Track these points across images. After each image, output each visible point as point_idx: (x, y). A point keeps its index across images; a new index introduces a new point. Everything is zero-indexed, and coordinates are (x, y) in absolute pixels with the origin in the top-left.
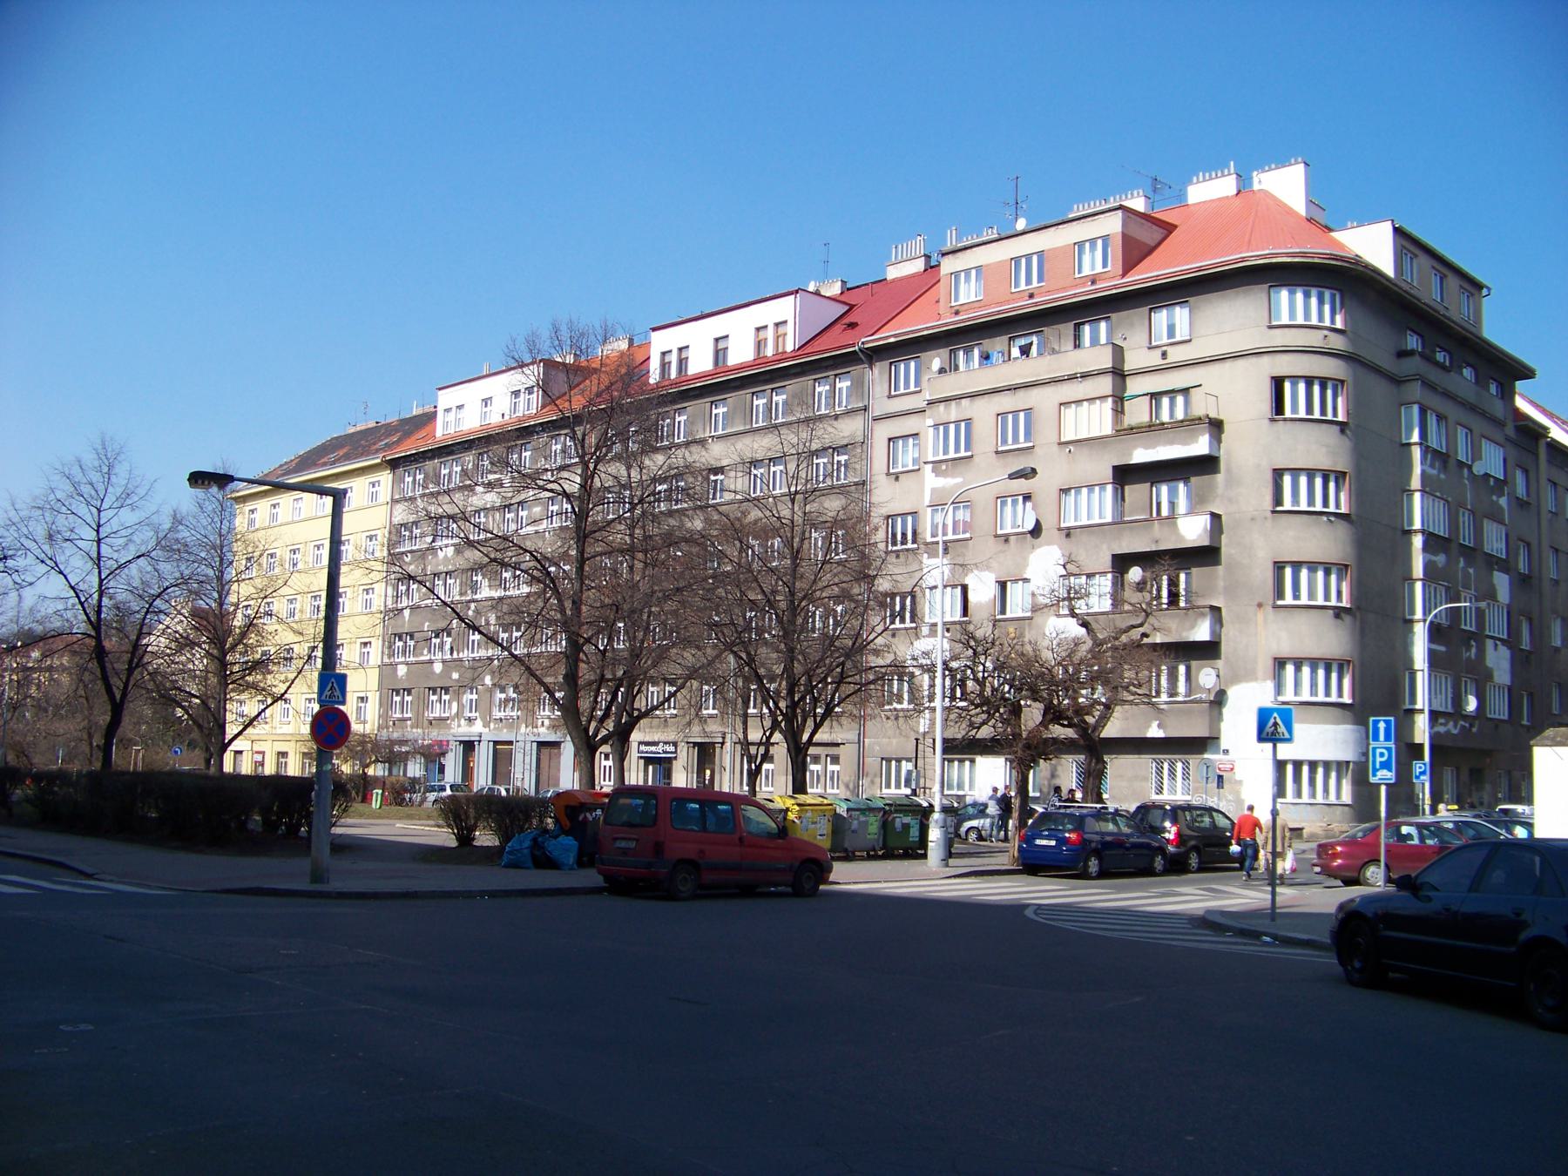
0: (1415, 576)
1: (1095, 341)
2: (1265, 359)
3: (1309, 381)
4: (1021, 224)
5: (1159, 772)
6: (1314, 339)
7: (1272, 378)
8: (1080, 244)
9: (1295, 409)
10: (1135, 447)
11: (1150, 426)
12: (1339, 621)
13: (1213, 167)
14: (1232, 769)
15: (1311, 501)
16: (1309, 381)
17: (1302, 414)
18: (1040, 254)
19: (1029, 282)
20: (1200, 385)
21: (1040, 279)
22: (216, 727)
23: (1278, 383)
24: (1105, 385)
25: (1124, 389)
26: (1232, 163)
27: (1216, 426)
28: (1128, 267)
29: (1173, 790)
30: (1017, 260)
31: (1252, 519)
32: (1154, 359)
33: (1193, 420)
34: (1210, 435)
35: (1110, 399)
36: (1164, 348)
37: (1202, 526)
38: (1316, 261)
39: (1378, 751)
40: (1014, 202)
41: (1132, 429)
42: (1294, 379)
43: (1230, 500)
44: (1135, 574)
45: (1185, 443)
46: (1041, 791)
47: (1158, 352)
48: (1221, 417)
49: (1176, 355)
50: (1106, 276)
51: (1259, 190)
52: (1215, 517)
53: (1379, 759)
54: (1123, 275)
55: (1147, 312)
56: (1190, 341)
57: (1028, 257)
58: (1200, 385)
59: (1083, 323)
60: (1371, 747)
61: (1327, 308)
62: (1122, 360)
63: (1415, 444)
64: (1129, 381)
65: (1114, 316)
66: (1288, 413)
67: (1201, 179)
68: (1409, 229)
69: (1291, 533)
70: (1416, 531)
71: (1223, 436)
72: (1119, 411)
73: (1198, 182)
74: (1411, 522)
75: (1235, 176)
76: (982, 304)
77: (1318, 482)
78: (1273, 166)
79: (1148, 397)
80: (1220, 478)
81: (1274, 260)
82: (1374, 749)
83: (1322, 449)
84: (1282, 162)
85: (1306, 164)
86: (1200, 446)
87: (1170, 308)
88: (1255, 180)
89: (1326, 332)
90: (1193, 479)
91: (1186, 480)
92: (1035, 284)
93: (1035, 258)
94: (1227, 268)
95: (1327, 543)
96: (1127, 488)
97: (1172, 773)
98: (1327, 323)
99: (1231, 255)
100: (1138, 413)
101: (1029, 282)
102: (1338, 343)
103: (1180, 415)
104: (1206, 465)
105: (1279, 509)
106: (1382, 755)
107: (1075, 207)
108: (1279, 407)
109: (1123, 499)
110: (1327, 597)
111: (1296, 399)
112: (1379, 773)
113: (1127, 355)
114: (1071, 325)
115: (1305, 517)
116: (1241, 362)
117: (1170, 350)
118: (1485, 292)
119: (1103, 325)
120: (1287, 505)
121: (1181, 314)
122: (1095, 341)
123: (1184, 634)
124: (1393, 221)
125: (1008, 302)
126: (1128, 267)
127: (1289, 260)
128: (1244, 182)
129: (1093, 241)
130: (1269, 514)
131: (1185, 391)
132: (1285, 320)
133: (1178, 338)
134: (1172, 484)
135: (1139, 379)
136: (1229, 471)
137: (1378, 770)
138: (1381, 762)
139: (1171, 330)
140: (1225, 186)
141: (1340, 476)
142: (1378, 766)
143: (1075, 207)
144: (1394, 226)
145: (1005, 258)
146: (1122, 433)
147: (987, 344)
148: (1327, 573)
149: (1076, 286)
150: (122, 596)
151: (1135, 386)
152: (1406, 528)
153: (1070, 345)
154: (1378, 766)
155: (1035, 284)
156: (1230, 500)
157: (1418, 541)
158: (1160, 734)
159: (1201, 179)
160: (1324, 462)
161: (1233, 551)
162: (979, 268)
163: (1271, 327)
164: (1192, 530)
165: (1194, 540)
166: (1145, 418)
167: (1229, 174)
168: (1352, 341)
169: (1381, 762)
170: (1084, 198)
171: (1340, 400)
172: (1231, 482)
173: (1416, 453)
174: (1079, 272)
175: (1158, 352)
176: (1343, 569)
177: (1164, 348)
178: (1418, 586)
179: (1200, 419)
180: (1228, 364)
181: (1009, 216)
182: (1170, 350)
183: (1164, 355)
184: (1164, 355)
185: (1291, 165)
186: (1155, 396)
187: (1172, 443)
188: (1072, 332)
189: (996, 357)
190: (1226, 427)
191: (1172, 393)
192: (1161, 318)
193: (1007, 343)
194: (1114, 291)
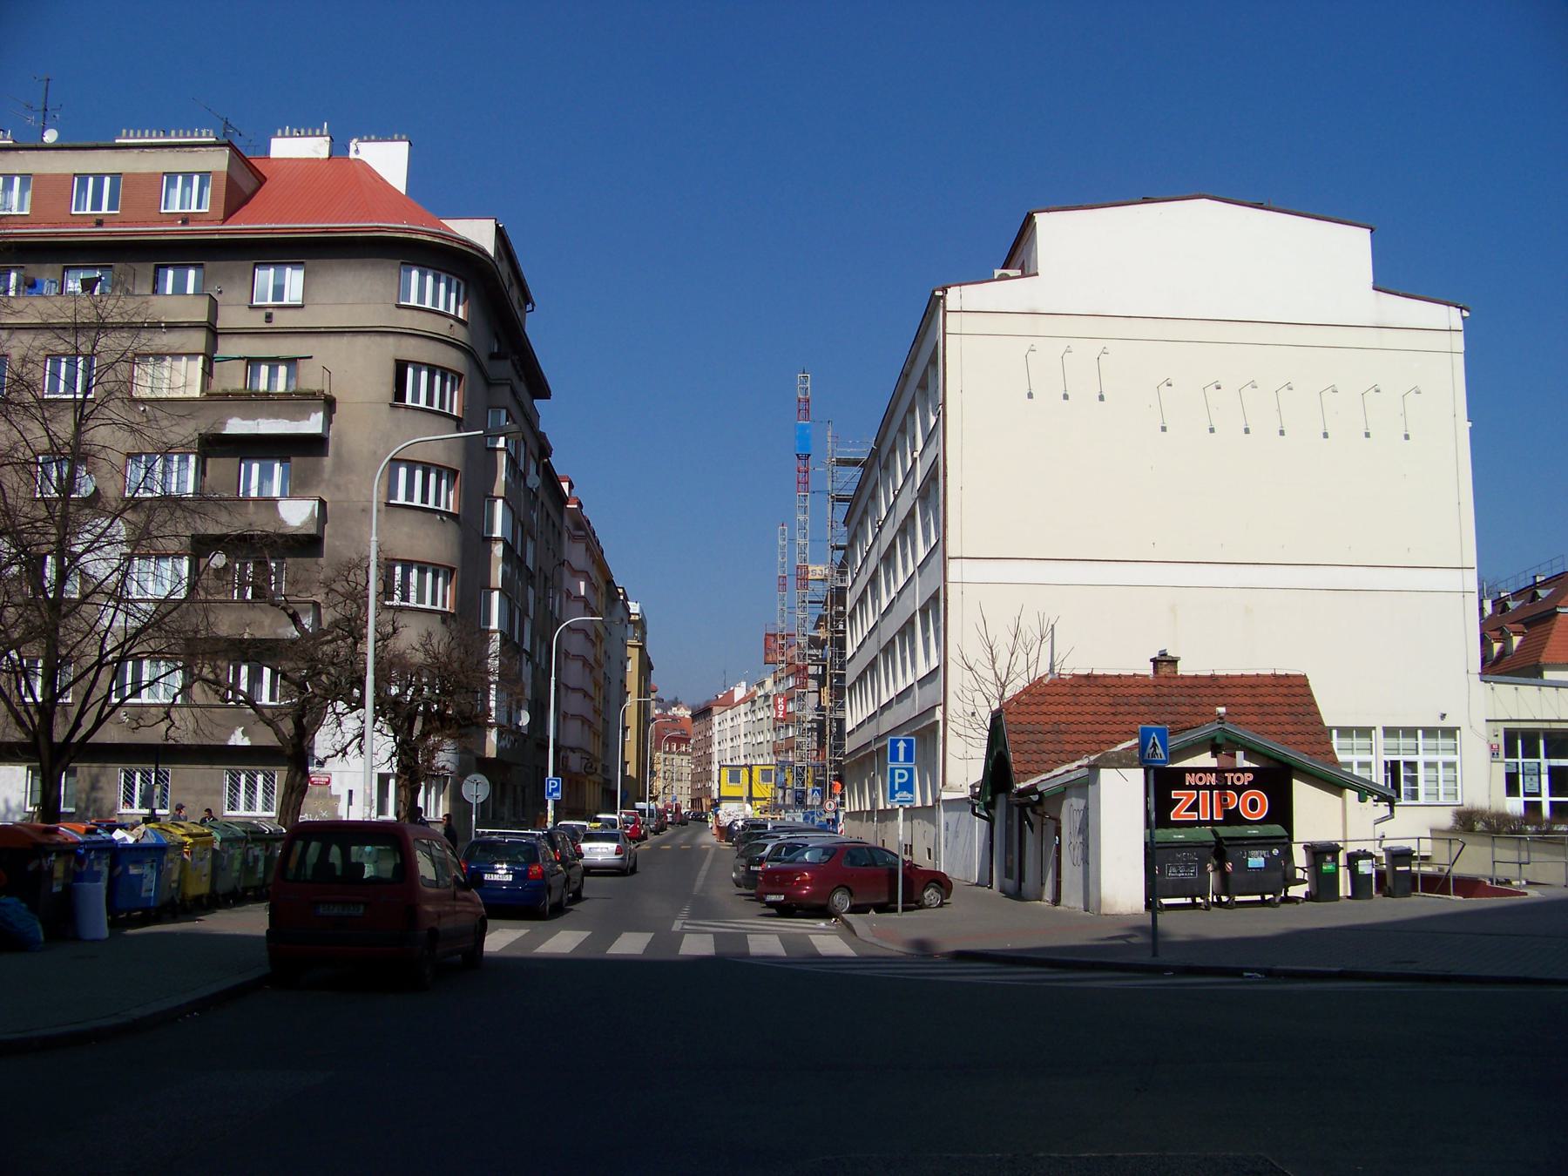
0: (493, 585)
1: (180, 288)
2: (391, 340)
3: (432, 370)
4: (50, 137)
5: (235, 785)
6: (441, 327)
7: (396, 360)
8: (172, 176)
9: (416, 398)
10: (231, 417)
11: (267, 394)
12: (444, 626)
13: (304, 125)
14: (328, 783)
15: (425, 499)
16: (432, 370)
17: (422, 404)
18: (115, 177)
19: (97, 204)
20: (311, 357)
21: (112, 206)
22: (714, 828)
23: (401, 367)
24: (198, 340)
25: (215, 349)
26: (326, 124)
27: (329, 404)
28: (231, 211)
29: (250, 805)
30: (83, 178)
31: (363, 510)
32: (257, 320)
33: (306, 394)
34: (324, 414)
35: (201, 358)
36: (270, 310)
37: (309, 510)
38: (455, 245)
39: (897, 772)
40: (42, 107)
41: (228, 394)
42: (418, 366)
43: (338, 487)
44: (219, 560)
45: (293, 419)
46: (77, 807)
47: (262, 314)
48: (334, 394)
49: (282, 320)
50: (200, 217)
51: (355, 159)
52: (322, 503)
53: (897, 781)
54: (224, 221)
55: (252, 266)
56: (302, 307)
57: (99, 178)
58: (311, 357)
59: (167, 267)
60: (889, 767)
61: (453, 296)
62: (216, 318)
63: (501, 449)
64: (221, 342)
65: (208, 264)
66: (408, 402)
67: (287, 133)
68: (511, 235)
69: (406, 529)
70: (496, 539)
71: (334, 416)
72: (207, 373)
73: (283, 136)
74: (491, 528)
75: (328, 139)
76: (28, 220)
77: (419, 474)
78: (373, 137)
79: (244, 363)
80: (328, 461)
81: (414, 236)
82: (893, 770)
83: (437, 442)
84: (384, 135)
85: (410, 144)
86: (313, 424)
87: (280, 267)
88: (352, 147)
89: (452, 322)
90: (294, 459)
91: (284, 459)
92: (105, 210)
93: (107, 180)
94: (360, 235)
95: (434, 544)
96: (209, 461)
97: (251, 785)
98: (452, 312)
99: (335, 222)
100: (231, 378)
101: (97, 204)
102: (461, 334)
103: (281, 387)
104: (313, 445)
105: (392, 502)
106: (901, 776)
107: (124, 131)
108: (400, 394)
109: (204, 473)
110: (434, 602)
111: (419, 387)
112: (898, 796)
113: (222, 311)
114: (151, 266)
115: (420, 513)
116: (362, 340)
117: (276, 313)
118: (529, 307)
119: (192, 273)
120: (401, 499)
121: (294, 280)
122: (180, 288)
123: (280, 631)
124: (496, 220)
125: (66, 225)
126: (231, 211)
127: (429, 239)
128: (339, 148)
129: (188, 177)
130: (383, 506)
131: (291, 362)
132: (413, 302)
133: (286, 302)
134: (269, 462)
135: (235, 340)
136: (338, 455)
137: (897, 792)
138: (899, 784)
139: (279, 291)
140: (314, 147)
141: (453, 473)
142: (897, 788)
143: (124, 131)
144: (497, 226)
145: (65, 171)
146: (215, 398)
147: (33, 270)
148: (422, 571)
149: (161, 223)
150: (100, 464)
151: (227, 347)
152: (485, 535)
153: (148, 291)
154: (897, 788)
155: (105, 210)
156: (338, 487)
157: (498, 550)
158: (246, 742)
159: (287, 133)
160: (438, 456)
161: (338, 543)
162: (26, 177)
163: (399, 307)
164: (296, 514)
165: (298, 528)
166: (239, 385)
167: (321, 135)
168: (472, 334)
169: (899, 784)
170: (140, 126)
171: (456, 393)
172: (341, 466)
173: (502, 459)
174: (165, 208)
175: (262, 314)
176: (449, 572)
177: (270, 310)
178: (496, 596)
179: (315, 394)
180: (345, 340)
181: (32, 120)
182: (276, 313)
183: (269, 318)
184: (269, 318)
185: (393, 140)
186: (253, 362)
187: (277, 417)
188: (152, 274)
189: (49, 288)
190: (338, 407)
191: (273, 362)
192: (266, 277)
193: (60, 273)
194: (217, 237)
